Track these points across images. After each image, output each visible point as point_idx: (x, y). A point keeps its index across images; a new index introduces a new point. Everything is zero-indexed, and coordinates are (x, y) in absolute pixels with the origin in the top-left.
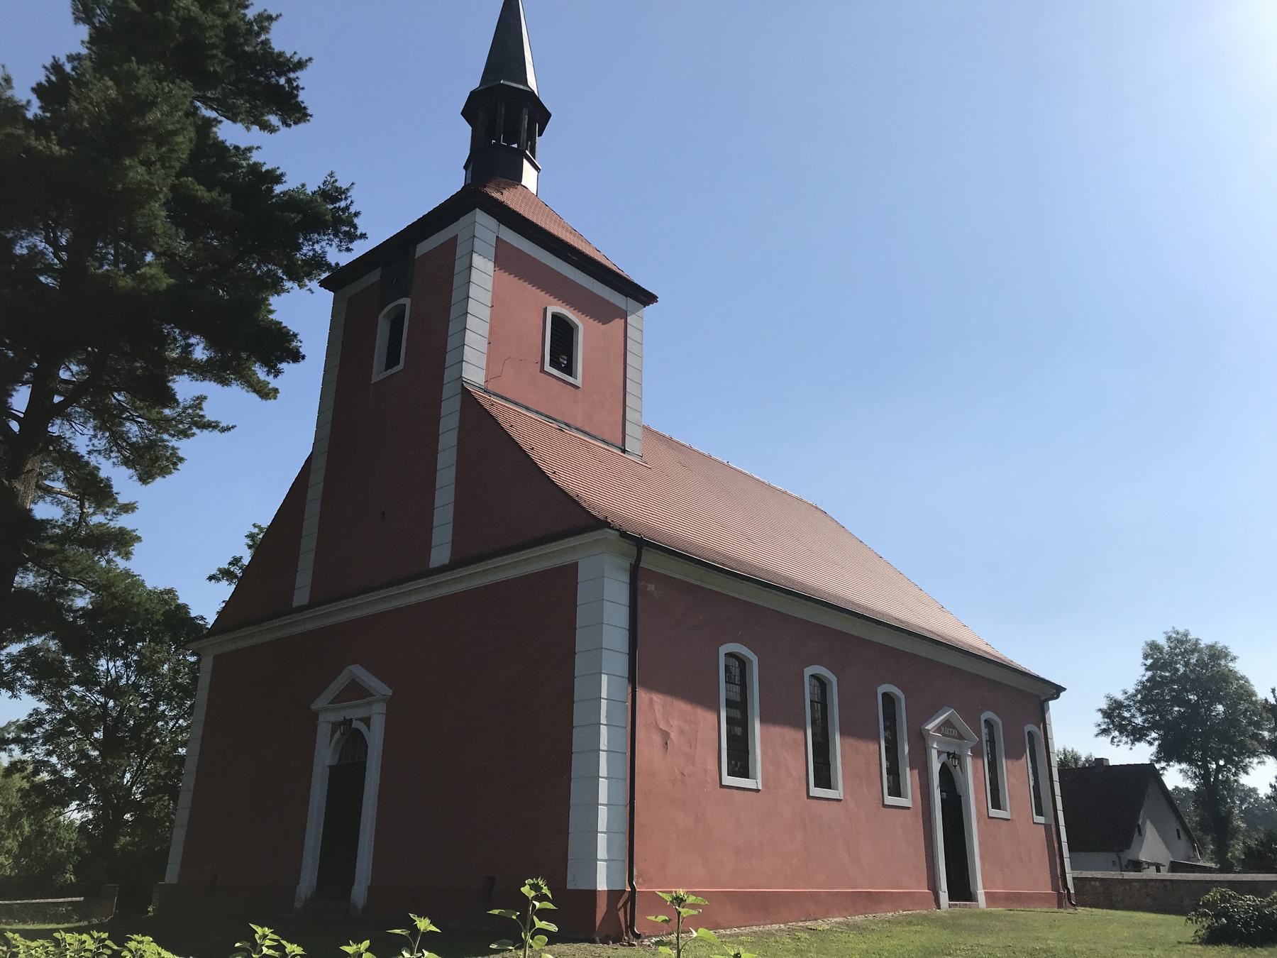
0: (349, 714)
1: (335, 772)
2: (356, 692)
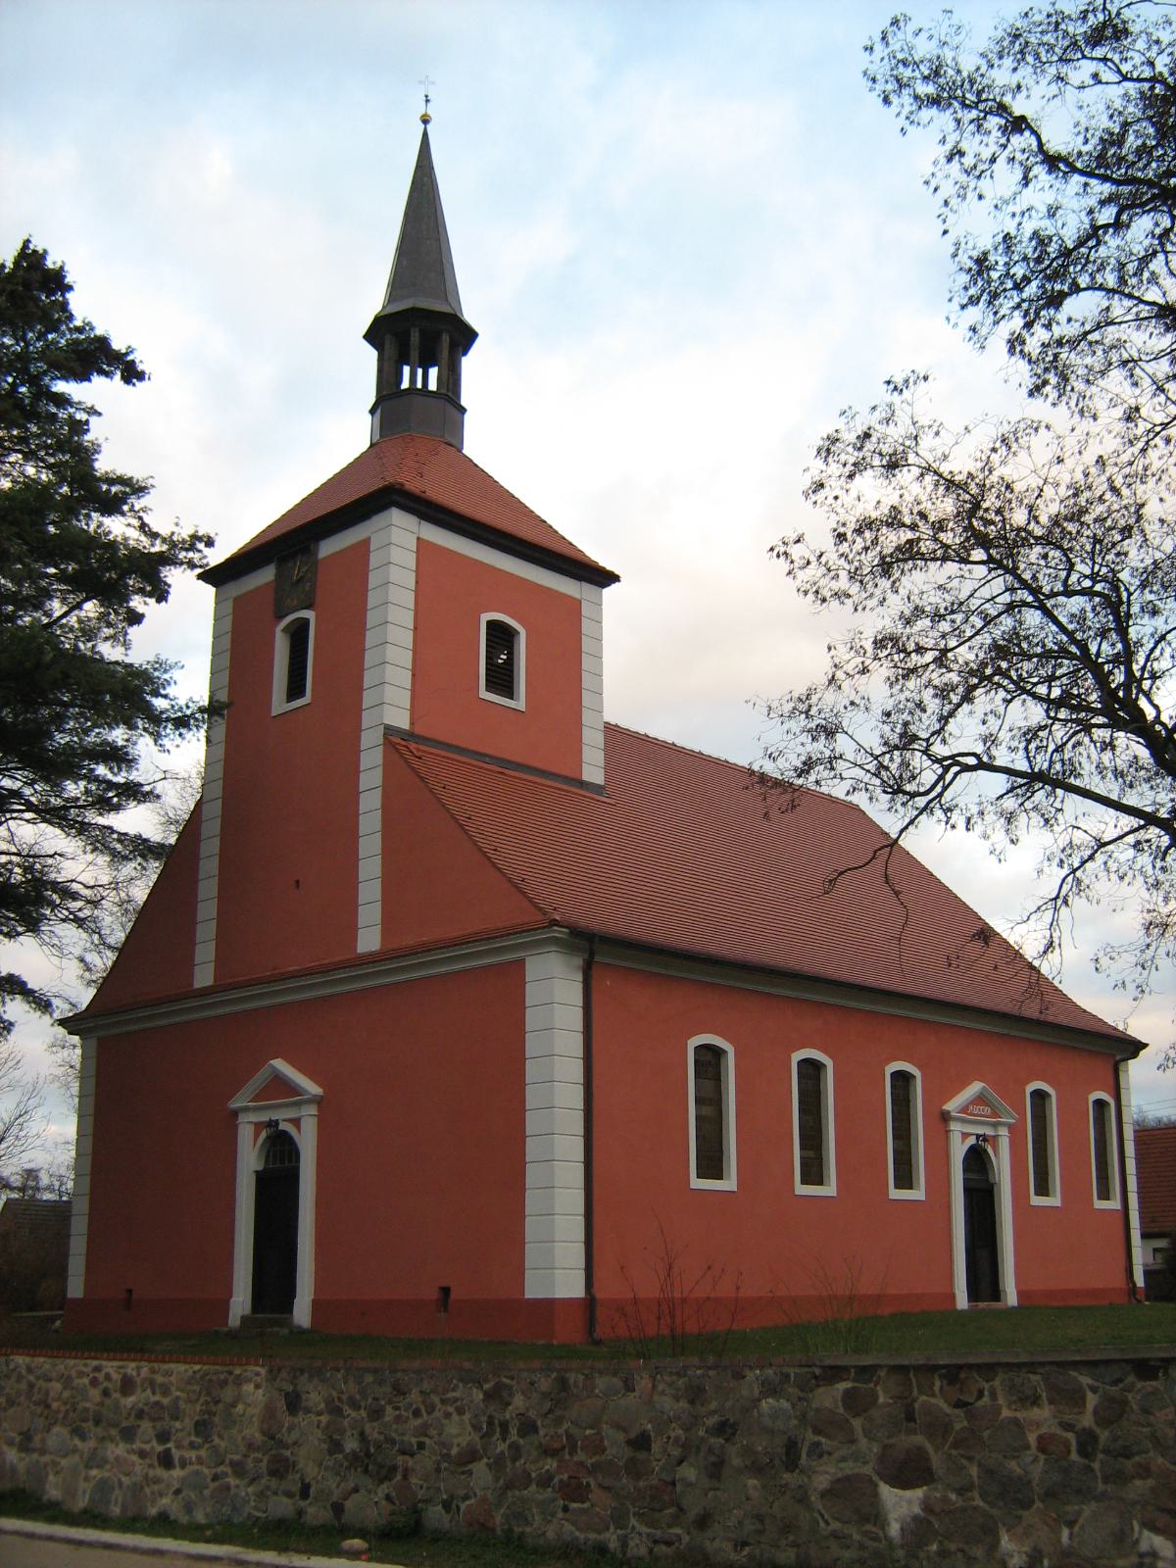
0: (275, 1116)
1: (262, 1179)
2: (281, 1087)
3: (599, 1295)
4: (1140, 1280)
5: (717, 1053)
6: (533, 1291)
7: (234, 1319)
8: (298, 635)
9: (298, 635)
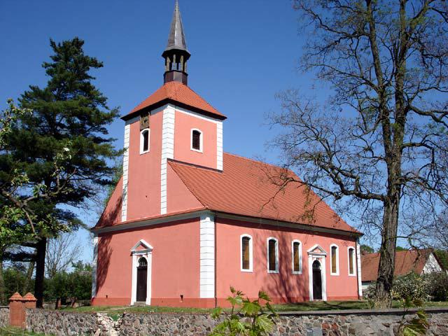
3: (217, 297)
4: (361, 294)
5: (248, 239)
6: (202, 296)
7: (132, 304)
8: (146, 134)
9: (146, 134)
